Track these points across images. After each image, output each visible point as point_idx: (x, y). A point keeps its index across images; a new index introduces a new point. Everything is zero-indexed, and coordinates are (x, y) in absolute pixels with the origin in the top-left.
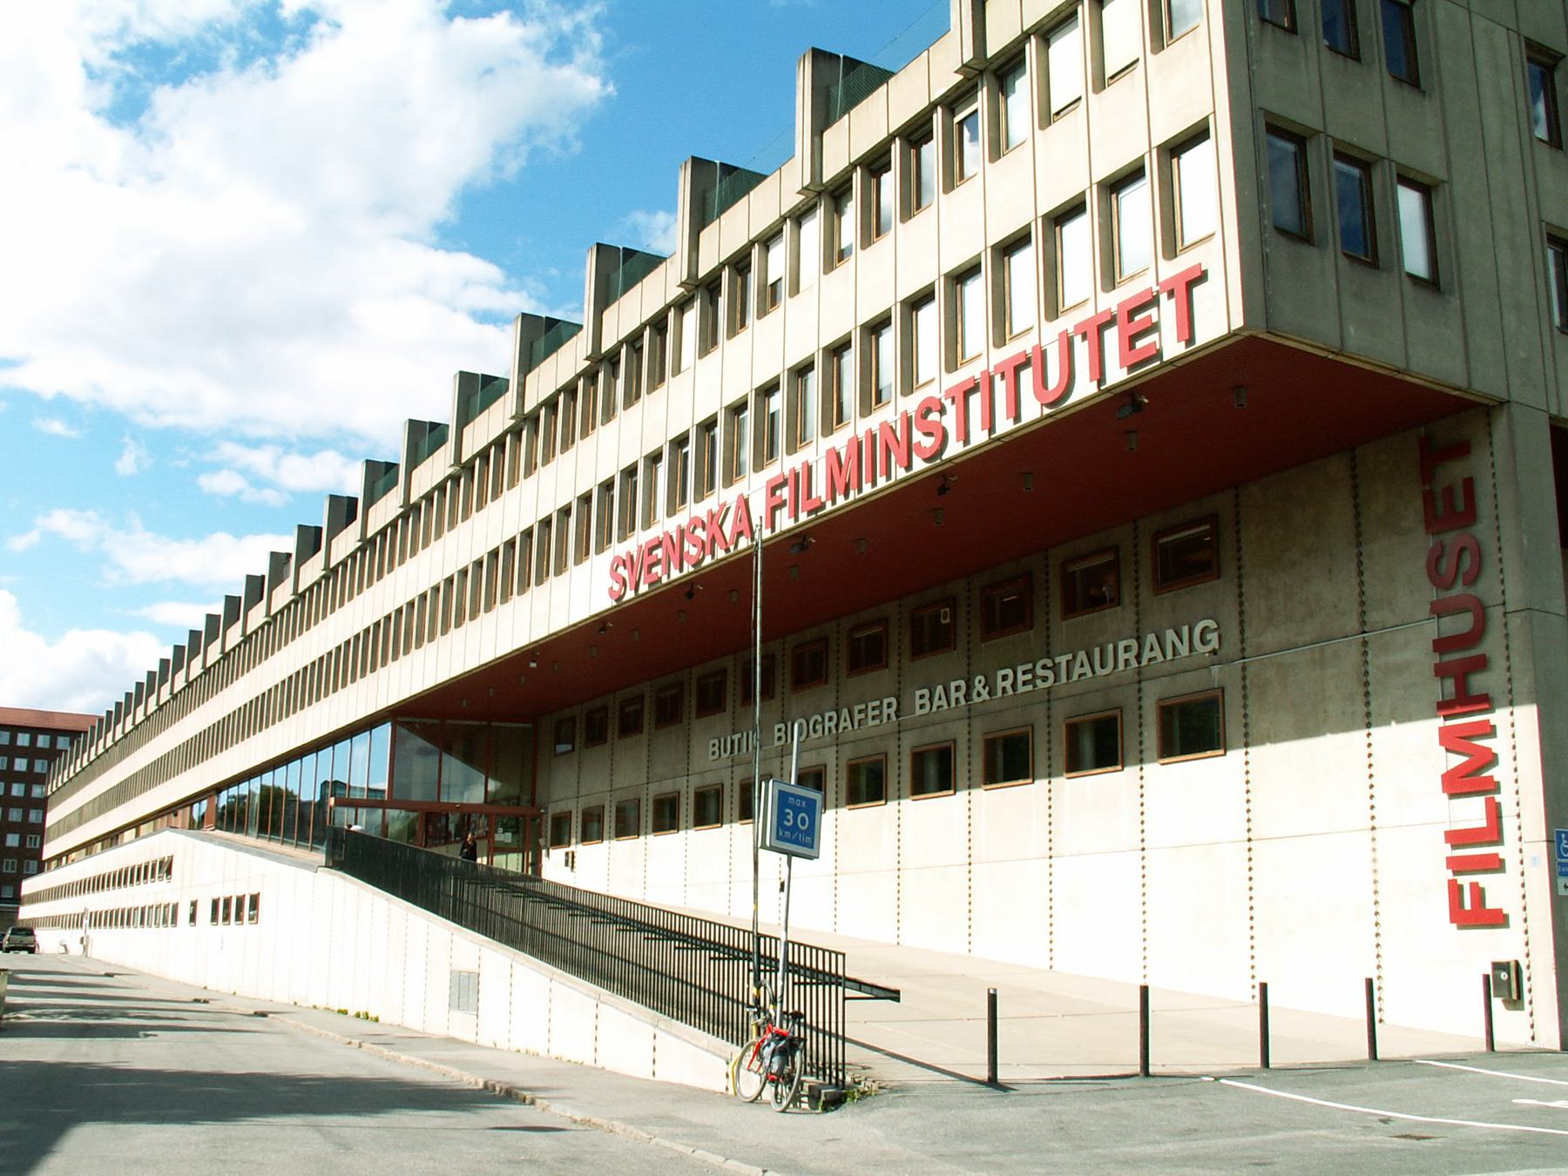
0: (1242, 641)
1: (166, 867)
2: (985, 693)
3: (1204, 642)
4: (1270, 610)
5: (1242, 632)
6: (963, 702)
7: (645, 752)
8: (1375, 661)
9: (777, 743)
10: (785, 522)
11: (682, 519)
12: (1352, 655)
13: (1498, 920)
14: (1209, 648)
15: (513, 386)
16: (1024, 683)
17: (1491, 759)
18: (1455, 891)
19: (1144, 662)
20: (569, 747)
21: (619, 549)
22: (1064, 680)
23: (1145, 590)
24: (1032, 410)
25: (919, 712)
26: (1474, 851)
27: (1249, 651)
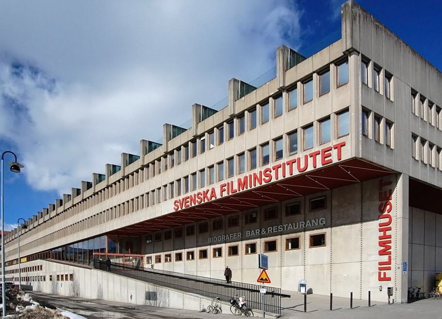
0: (331, 222)
1: (40, 268)
2: (265, 233)
3: (322, 222)
4: (339, 216)
5: (331, 220)
6: (259, 234)
7: (172, 243)
9: (209, 242)
10: (225, 194)
11: (196, 192)
13: (389, 279)
15: (141, 158)
17: (390, 248)
18: (380, 274)
19: (306, 226)
20: (150, 241)
21: (176, 198)
24: (296, 172)
25: (247, 236)
26: (384, 266)
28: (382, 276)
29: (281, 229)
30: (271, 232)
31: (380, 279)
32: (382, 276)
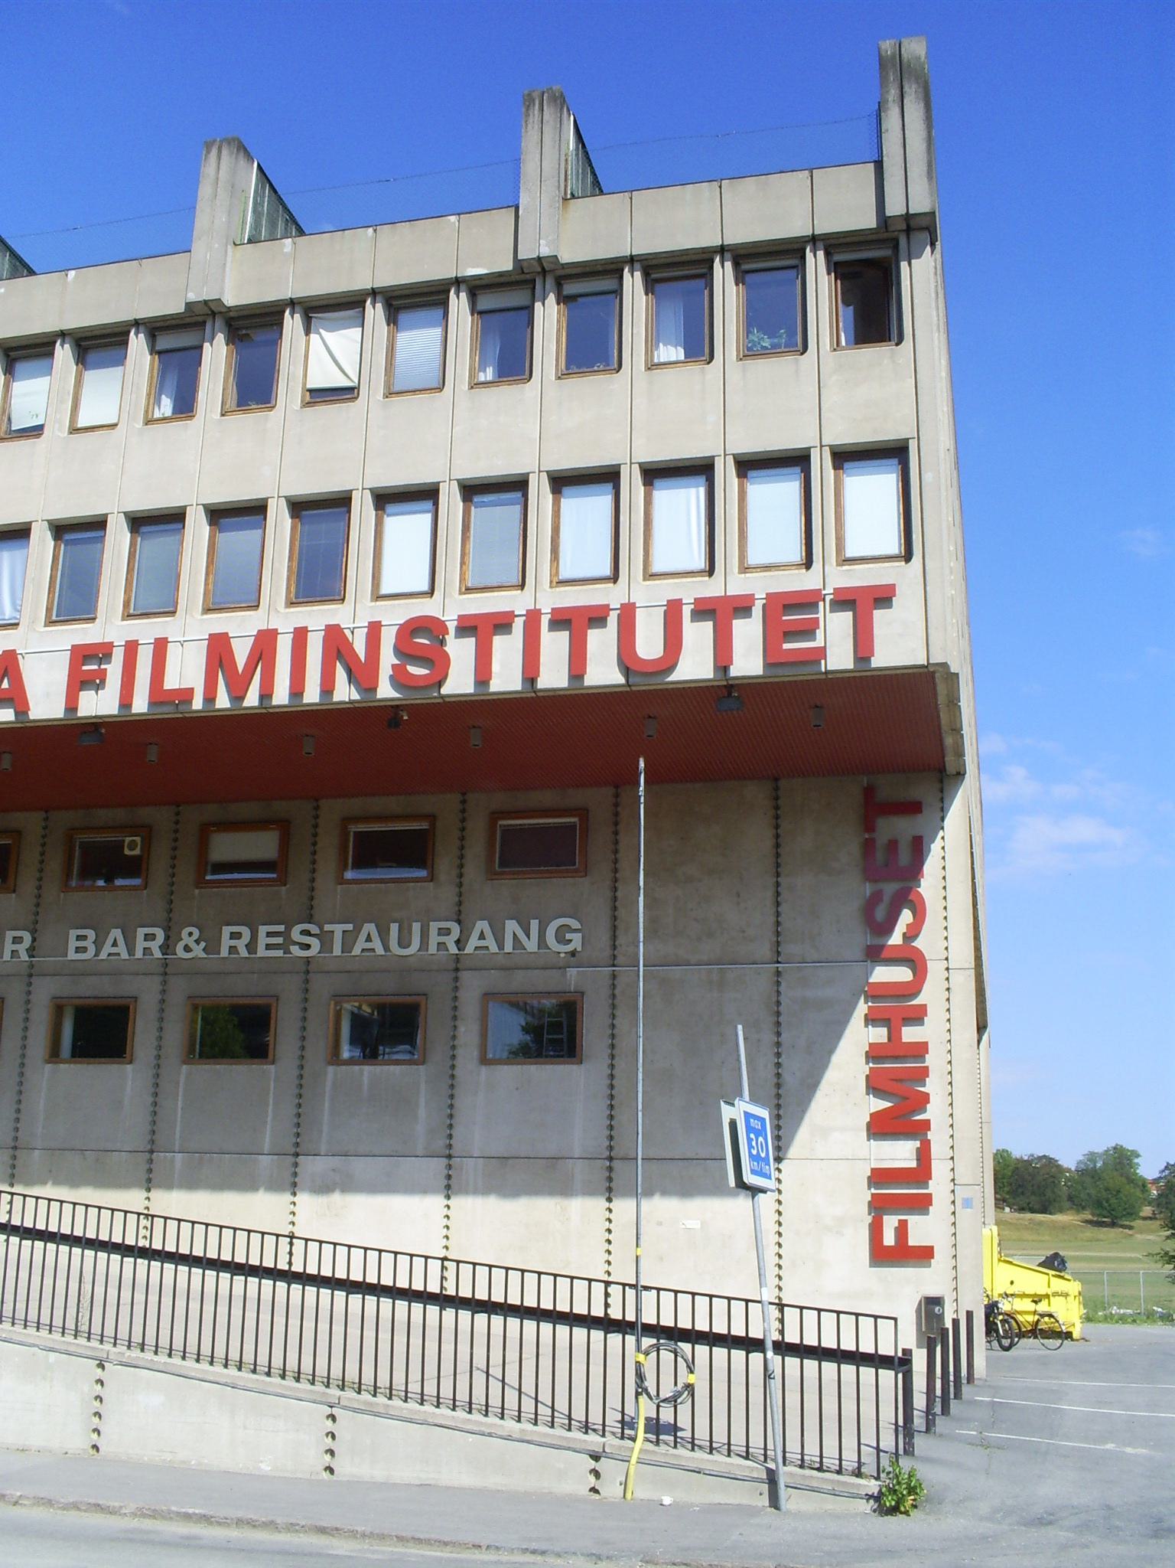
0: (614, 947)
2: (198, 951)
3: (561, 939)
5: (614, 938)
8: (788, 994)
12: (759, 981)
13: (924, 1254)
14: (570, 948)
16: (268, 947)
18: (876, 1230)
22: (337, 951)
23: (474, 871)
25: (72, 955)
27: (620, 960)
28: (889, 1239)
29: (308, 947)
30: (244, 953)
31: (881, 1255)
32: (889, 1239)
